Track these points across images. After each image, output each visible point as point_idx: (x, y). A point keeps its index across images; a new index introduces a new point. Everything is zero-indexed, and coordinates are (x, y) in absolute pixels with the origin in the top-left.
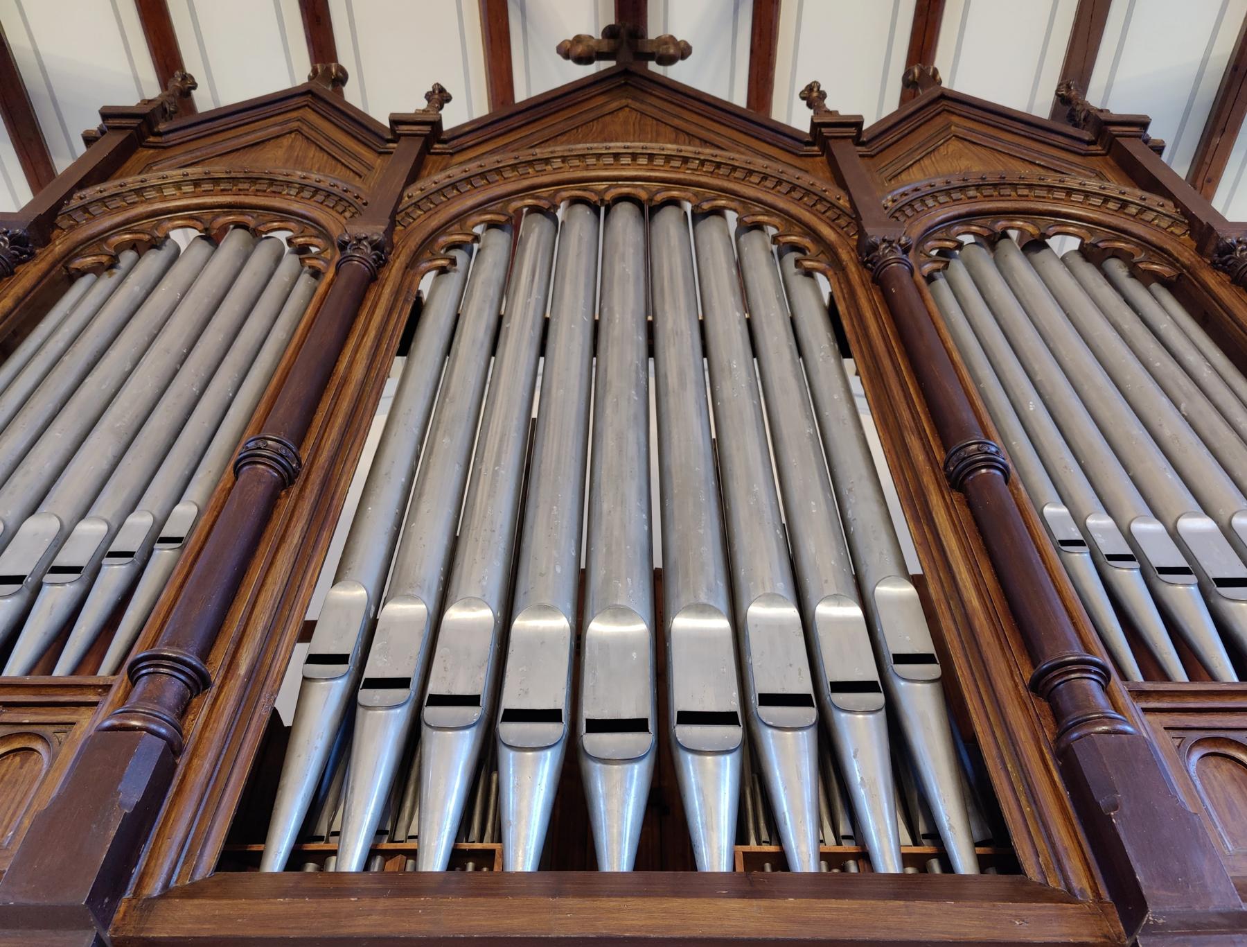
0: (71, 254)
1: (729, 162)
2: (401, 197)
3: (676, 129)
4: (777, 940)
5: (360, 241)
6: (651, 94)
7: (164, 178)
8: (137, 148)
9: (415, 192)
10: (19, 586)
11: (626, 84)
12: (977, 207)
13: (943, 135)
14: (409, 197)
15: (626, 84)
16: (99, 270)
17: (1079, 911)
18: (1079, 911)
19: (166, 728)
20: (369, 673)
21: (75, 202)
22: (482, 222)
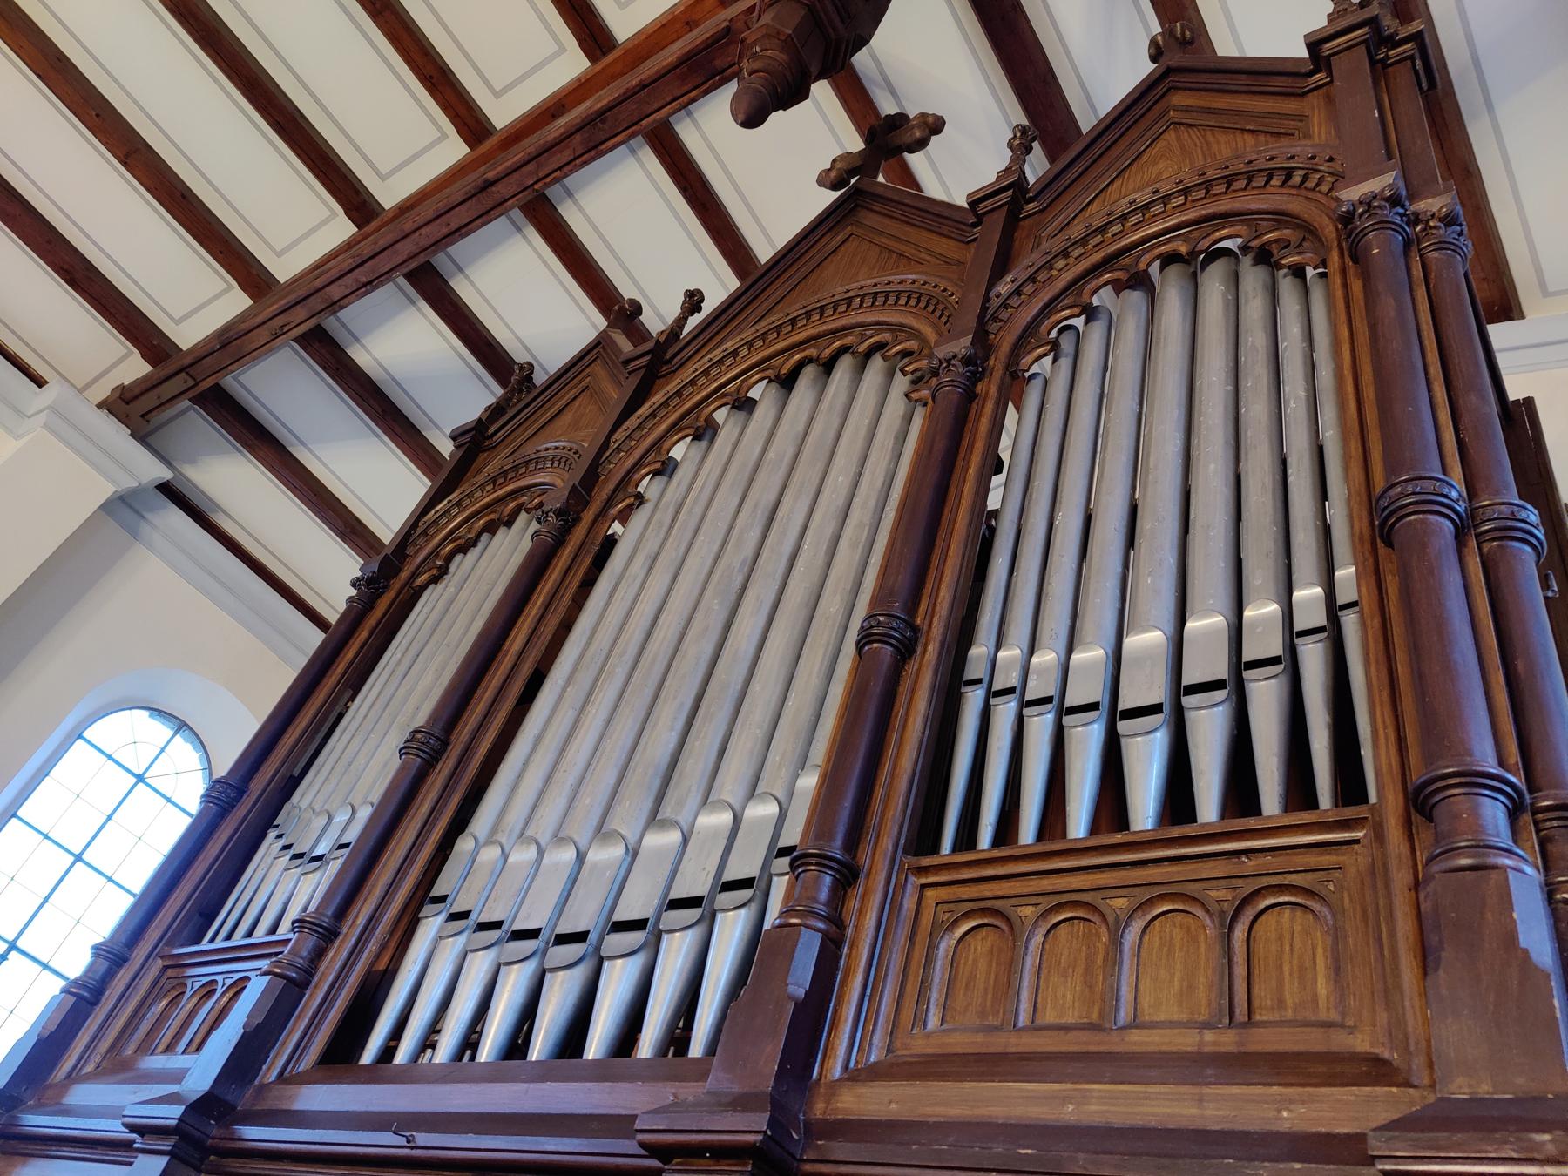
0: (415, 575)
1: (771, 327)
2: (986, 299)
3: (883, 248)
4: (505, 1114)
5: (948, 361)
6: (872, 210)
7: (1030, 266)
8: (654, 383)
9: (1004, 288)
10: (320, 863)
11: (856, 206)
12: (1115, 247)
13: (1151, 132)
14: (997, 297)
15: (856, 206)
16: (435, 580)
17: (1452, 840)
18: (1452, 840)
19: (297, 973)
20: (1028, 697)
21: (995, 303)
22: (1157, 257)
